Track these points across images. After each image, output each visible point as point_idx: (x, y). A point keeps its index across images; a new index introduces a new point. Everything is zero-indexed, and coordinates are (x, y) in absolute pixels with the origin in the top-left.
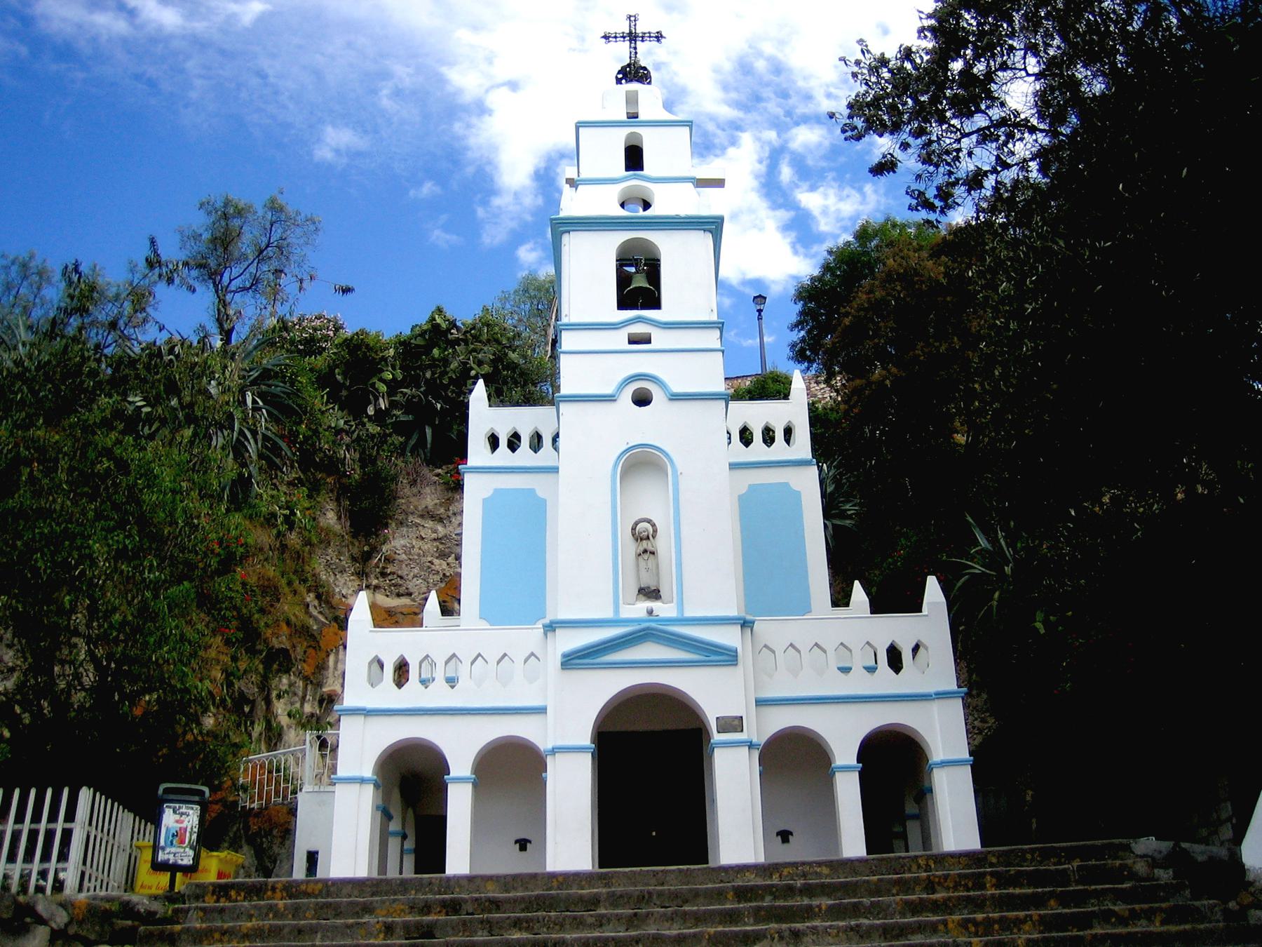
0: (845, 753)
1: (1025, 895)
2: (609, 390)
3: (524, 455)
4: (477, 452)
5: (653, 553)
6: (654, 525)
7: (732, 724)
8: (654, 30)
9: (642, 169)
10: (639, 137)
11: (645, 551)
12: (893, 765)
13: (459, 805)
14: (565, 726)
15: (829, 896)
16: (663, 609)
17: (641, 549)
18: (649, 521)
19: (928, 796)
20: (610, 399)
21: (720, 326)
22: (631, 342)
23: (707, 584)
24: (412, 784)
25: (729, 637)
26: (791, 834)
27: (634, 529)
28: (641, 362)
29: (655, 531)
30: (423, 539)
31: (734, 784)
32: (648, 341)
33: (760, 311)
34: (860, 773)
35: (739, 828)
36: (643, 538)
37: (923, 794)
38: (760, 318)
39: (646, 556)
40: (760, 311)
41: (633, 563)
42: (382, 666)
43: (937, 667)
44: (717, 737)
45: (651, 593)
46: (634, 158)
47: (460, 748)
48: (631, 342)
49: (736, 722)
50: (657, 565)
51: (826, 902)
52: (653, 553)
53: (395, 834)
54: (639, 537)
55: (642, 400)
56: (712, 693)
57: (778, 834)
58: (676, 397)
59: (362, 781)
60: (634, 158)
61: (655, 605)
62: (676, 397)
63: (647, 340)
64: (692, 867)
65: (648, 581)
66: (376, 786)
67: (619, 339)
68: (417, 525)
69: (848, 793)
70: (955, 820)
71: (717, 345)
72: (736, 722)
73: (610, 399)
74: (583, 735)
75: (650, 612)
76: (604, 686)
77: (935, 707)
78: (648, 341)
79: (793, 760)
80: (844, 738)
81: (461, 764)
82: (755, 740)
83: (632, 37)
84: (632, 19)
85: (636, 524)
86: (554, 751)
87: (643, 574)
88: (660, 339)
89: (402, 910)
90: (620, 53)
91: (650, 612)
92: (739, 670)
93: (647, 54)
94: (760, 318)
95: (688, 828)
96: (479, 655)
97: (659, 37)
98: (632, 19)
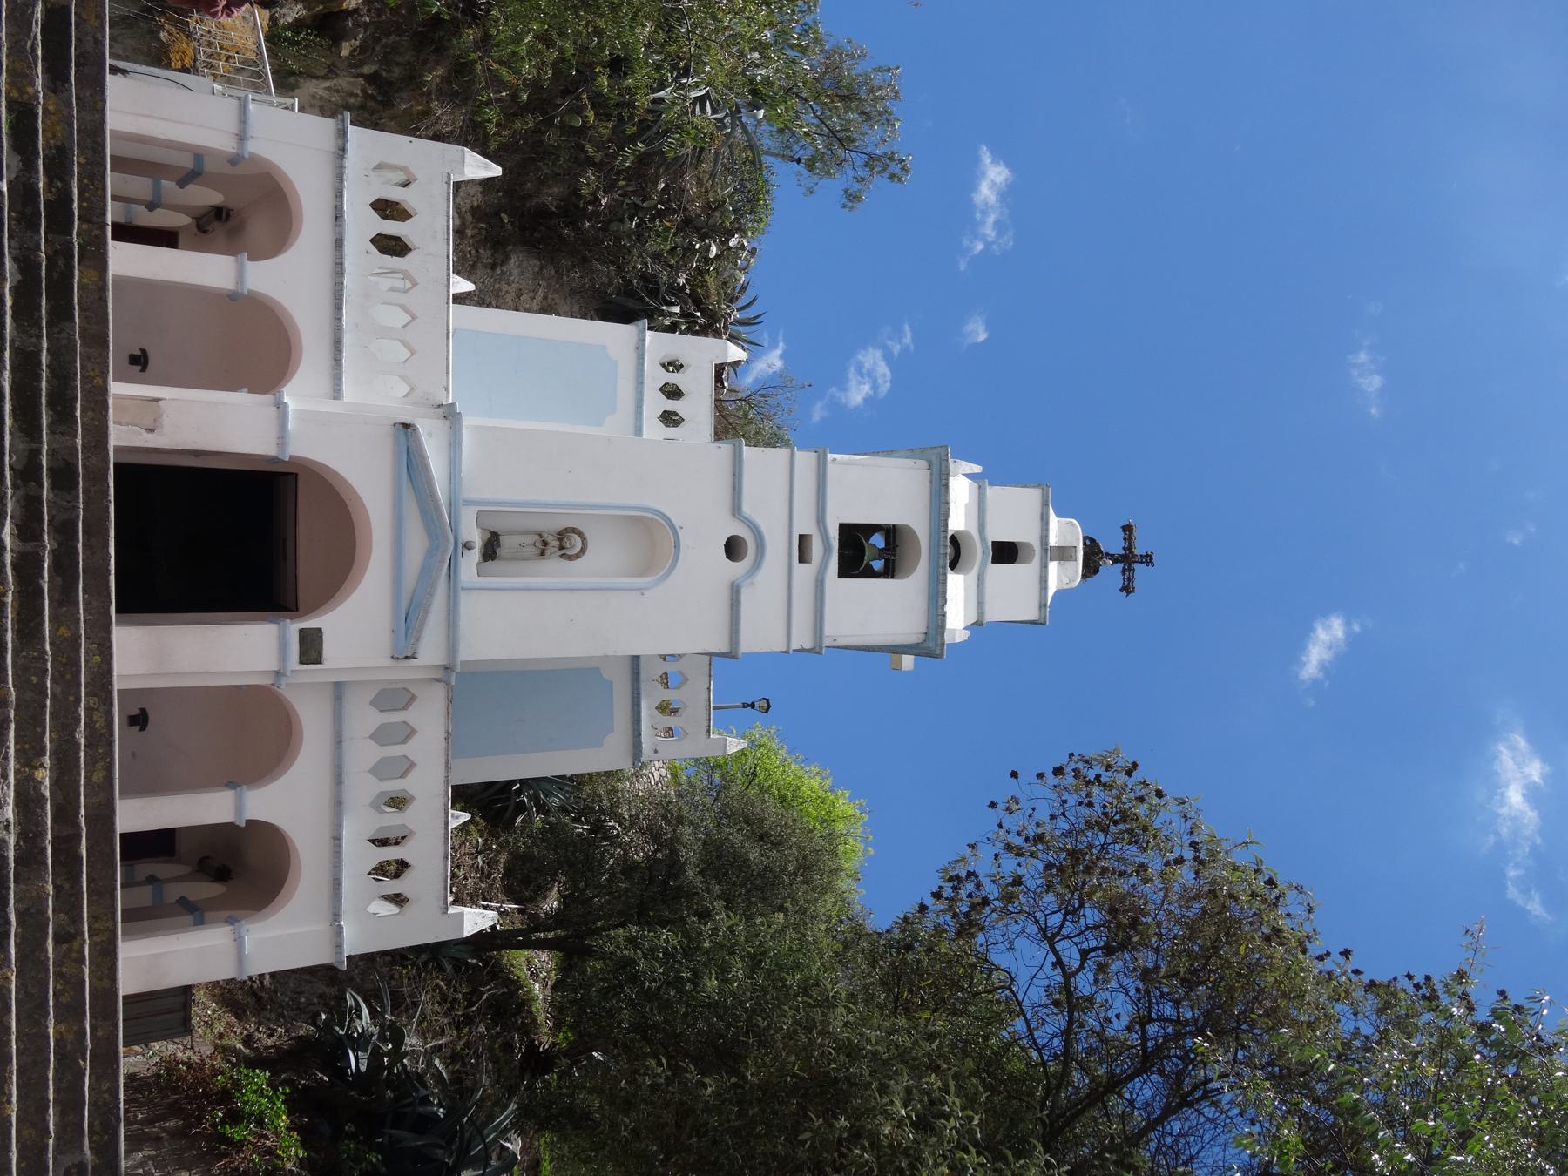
0: (263, 804)
1: (47, 1123)
2: (746, 509)
3: (656, 403)
4: (659, 344)
5: (542, 553)
6: (578, 556)
7: (311, 649)
8: (1137, 584)
9: (994, 561)
10: (1027, 560)
11: (545, 543)
12: (238, 869)
13: (204, 269)
14: (312, 419)
15: (55, 783)
16: (470, 562)
17: (549, 539)
18: (583, 551)
19: (190, 918)
20: (736, 509)
21: (731, 655)
22: (801, 537)
23: (507, 621)
24: (238, 210)
25: (431, 652)
26: (143, 729)
27: (574, 530)
28: (778, 548)
29: (570, 558)
30: (519, 297)
31: (239, 649)
32: (801, 560)
33: (752, 706)
34: (231, 825)
35: (154, 654)
36: (562, 542)
37: (195, 913)
38: (745, 706)
39: (539, 544)
40: (752, 706)
41: (544, 524)
42: (405, 185)
43: (371, 926)
44: (294, 628)
45: (491, 549)
46: (1006, 552)
47: (286, 279)
48: (801, 537)
49: (314, 655)
50: (524, 559)
51: (44, 776)
52: (542, 553)
53: (157, 189)
54: (562, 535)
55: (733, 548)
56: (355, 625)
57: (143, 711)
58: (735, 591)
59: (242, 137)
60: (1006, 552)
61: (475, 555)
62: (735, 591)
63: (803, 558)
64: (112, 578)
65: (507, 544)
66: (234, 160)
67: (804, 525)
68: (535, 292)
69: (207, 808)
70: (149, 961)
71: (795, 646)
72: (314, 655)
73: (736, 509)
74: (305, 446)
75: (468, 546)
76: (368, 480)
77: (321, 927)
78: (801, 560)
79: (252, 731)
80: (283, 802)
81: (266, 277)
82: (284, 681)
83: (1127, 559)
84: (1147, 559)
85: (580, 534)
86: (280, 406)
87: (518, 540)
88: (804, 573)
89: (54, 137)
90: (1112, 543)
91: (468, 546)
92: (388, 662)
93: (1111, 573)
94: (745, 706)
95: (156, 591)
96: (414, 318)
97: (1127, 589)
98: (1147, 559)
